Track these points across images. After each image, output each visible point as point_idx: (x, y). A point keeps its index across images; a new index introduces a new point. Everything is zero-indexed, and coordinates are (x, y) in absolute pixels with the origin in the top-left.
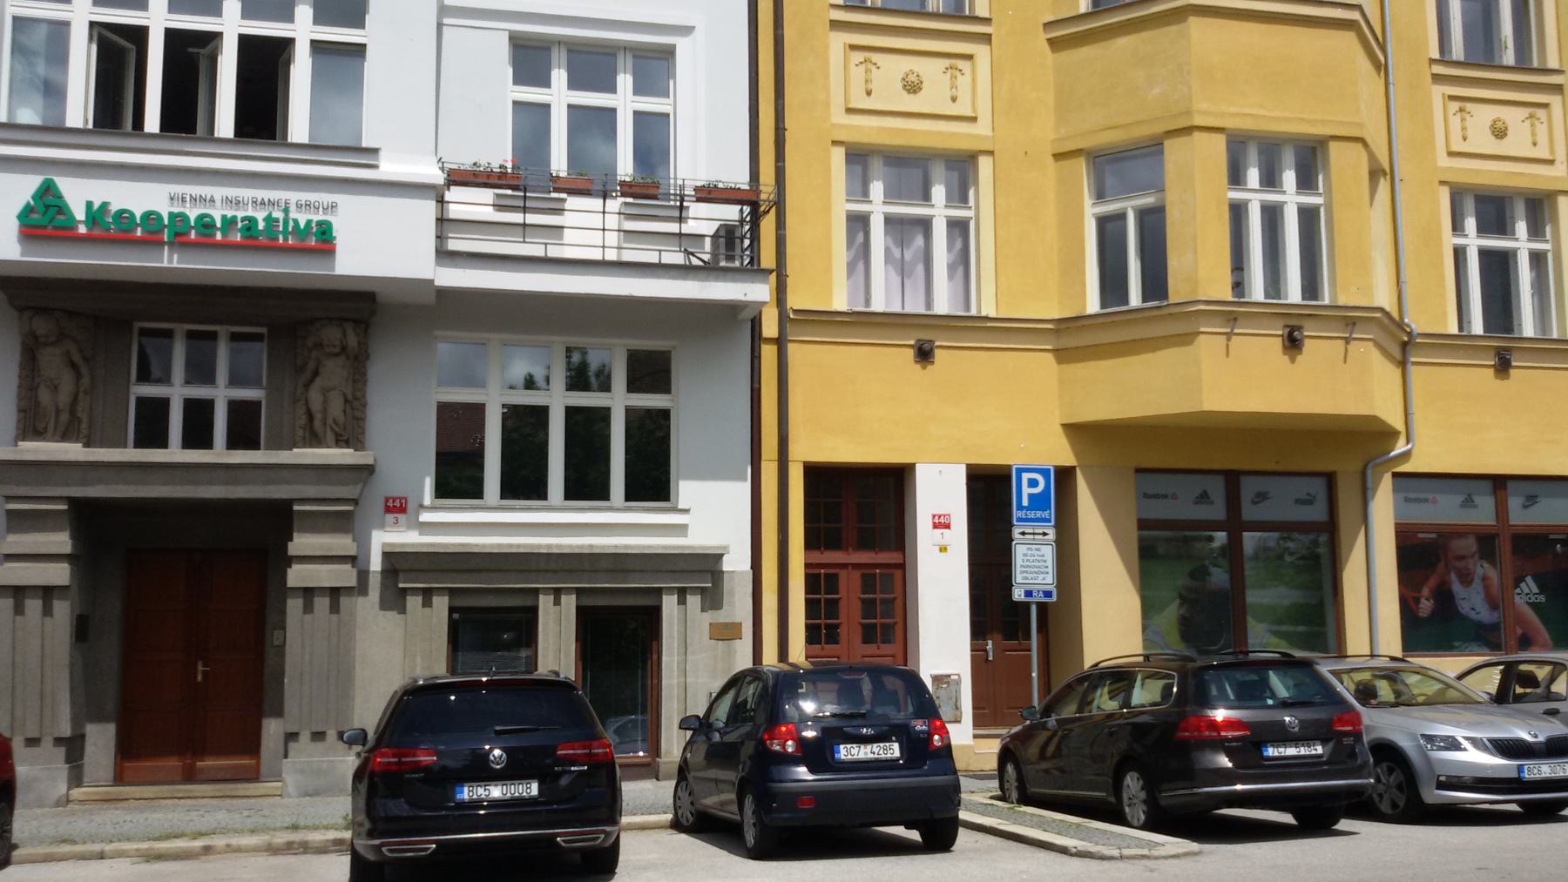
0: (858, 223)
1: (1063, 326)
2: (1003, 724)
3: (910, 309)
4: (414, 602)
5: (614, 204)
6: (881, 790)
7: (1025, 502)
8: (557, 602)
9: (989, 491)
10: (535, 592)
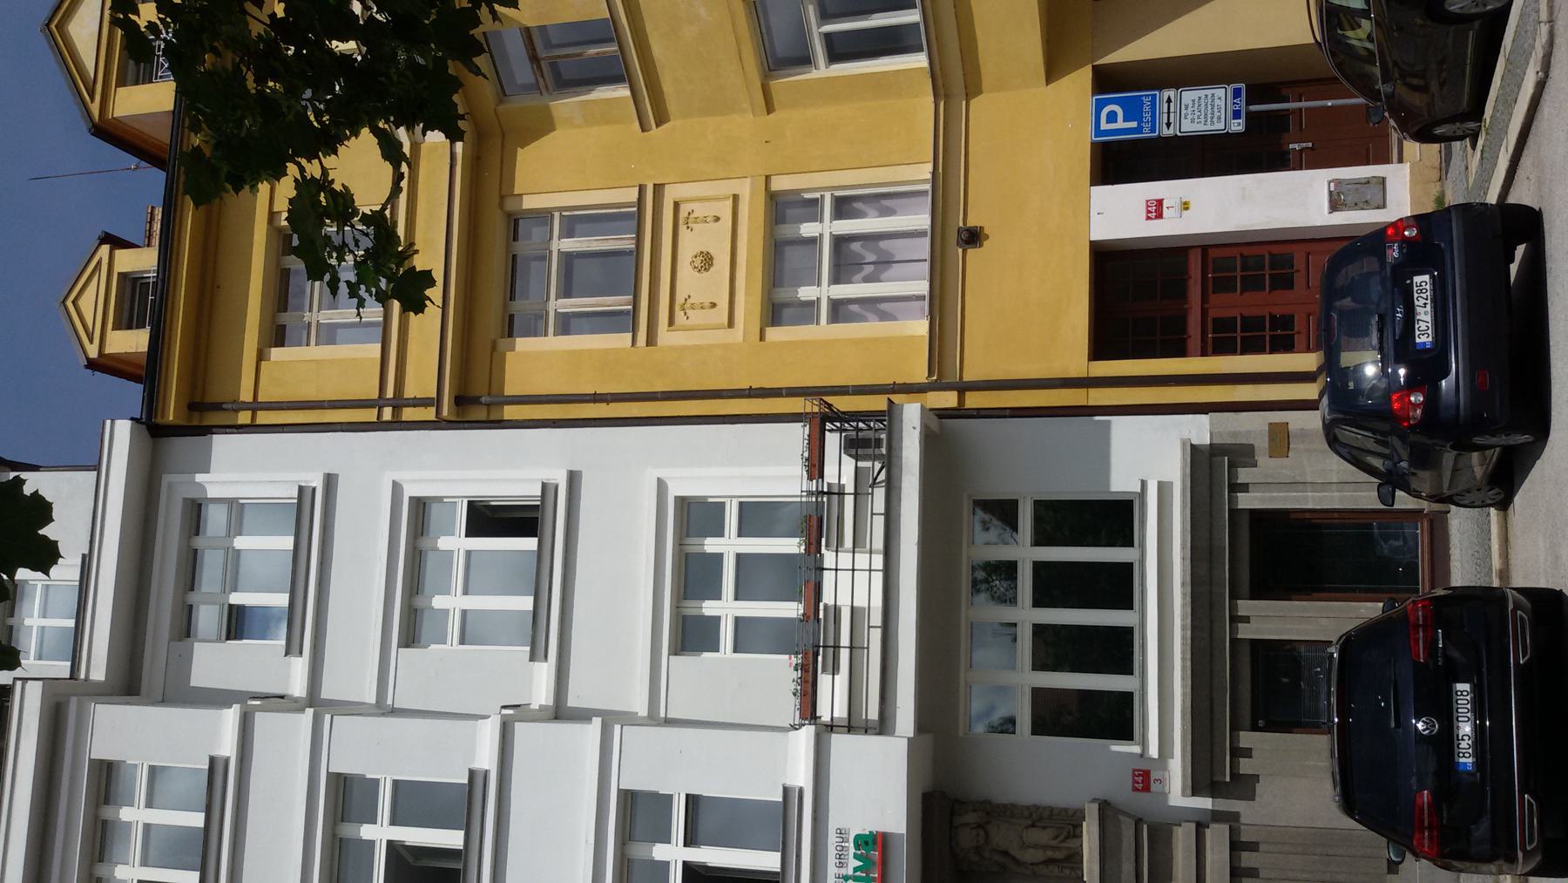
0: (839, 310)
1: (942, 92)
2: (1387, 136)
3: (925, 253)
4: (1245, 766)
5: (829, 558)
6: (1468, 296)
7: (1134, 124)
8: (1246, 619)
9: (1116, 162)
10: (1234, 512)
